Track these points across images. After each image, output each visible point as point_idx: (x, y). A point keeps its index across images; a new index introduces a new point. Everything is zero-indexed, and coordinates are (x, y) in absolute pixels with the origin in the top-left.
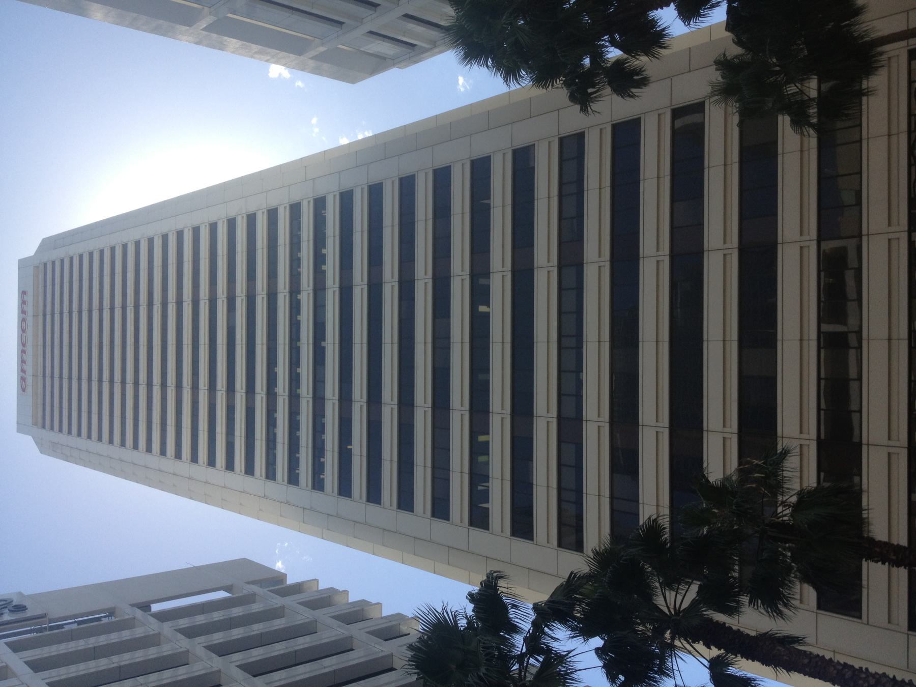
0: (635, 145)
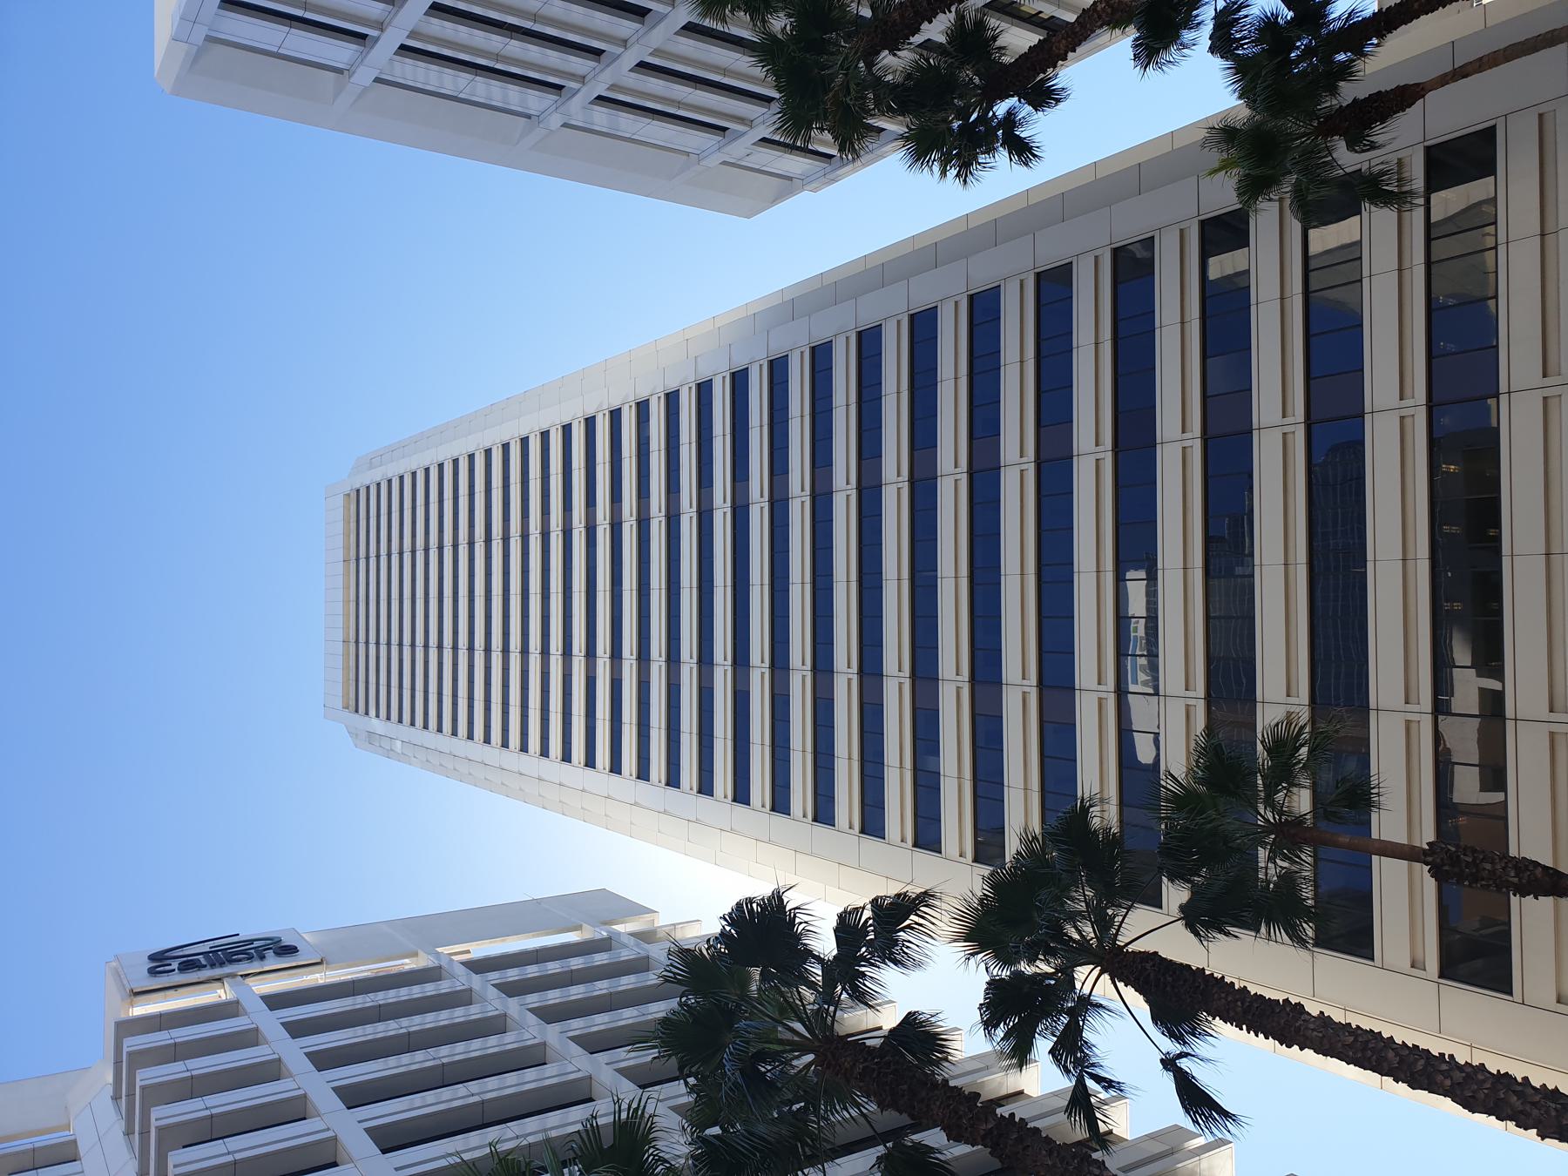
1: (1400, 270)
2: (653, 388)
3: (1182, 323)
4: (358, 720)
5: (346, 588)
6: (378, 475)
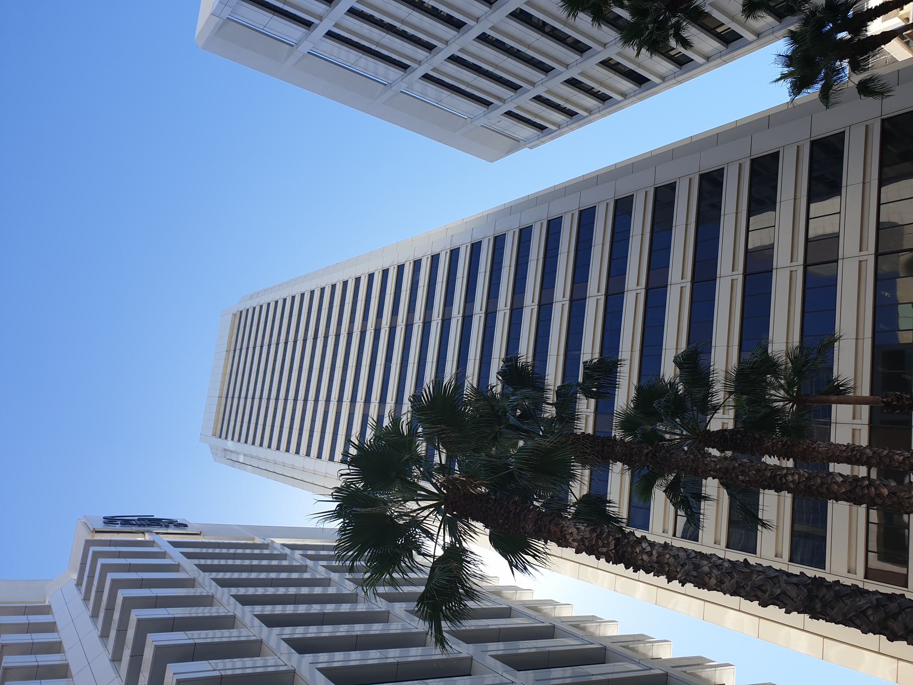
0: (671, 204)
1: (864, 183)
2: (424, 253)
3: (737, 213)
4: (221, 443)
5: (226, 367)
6: (255, 303)
